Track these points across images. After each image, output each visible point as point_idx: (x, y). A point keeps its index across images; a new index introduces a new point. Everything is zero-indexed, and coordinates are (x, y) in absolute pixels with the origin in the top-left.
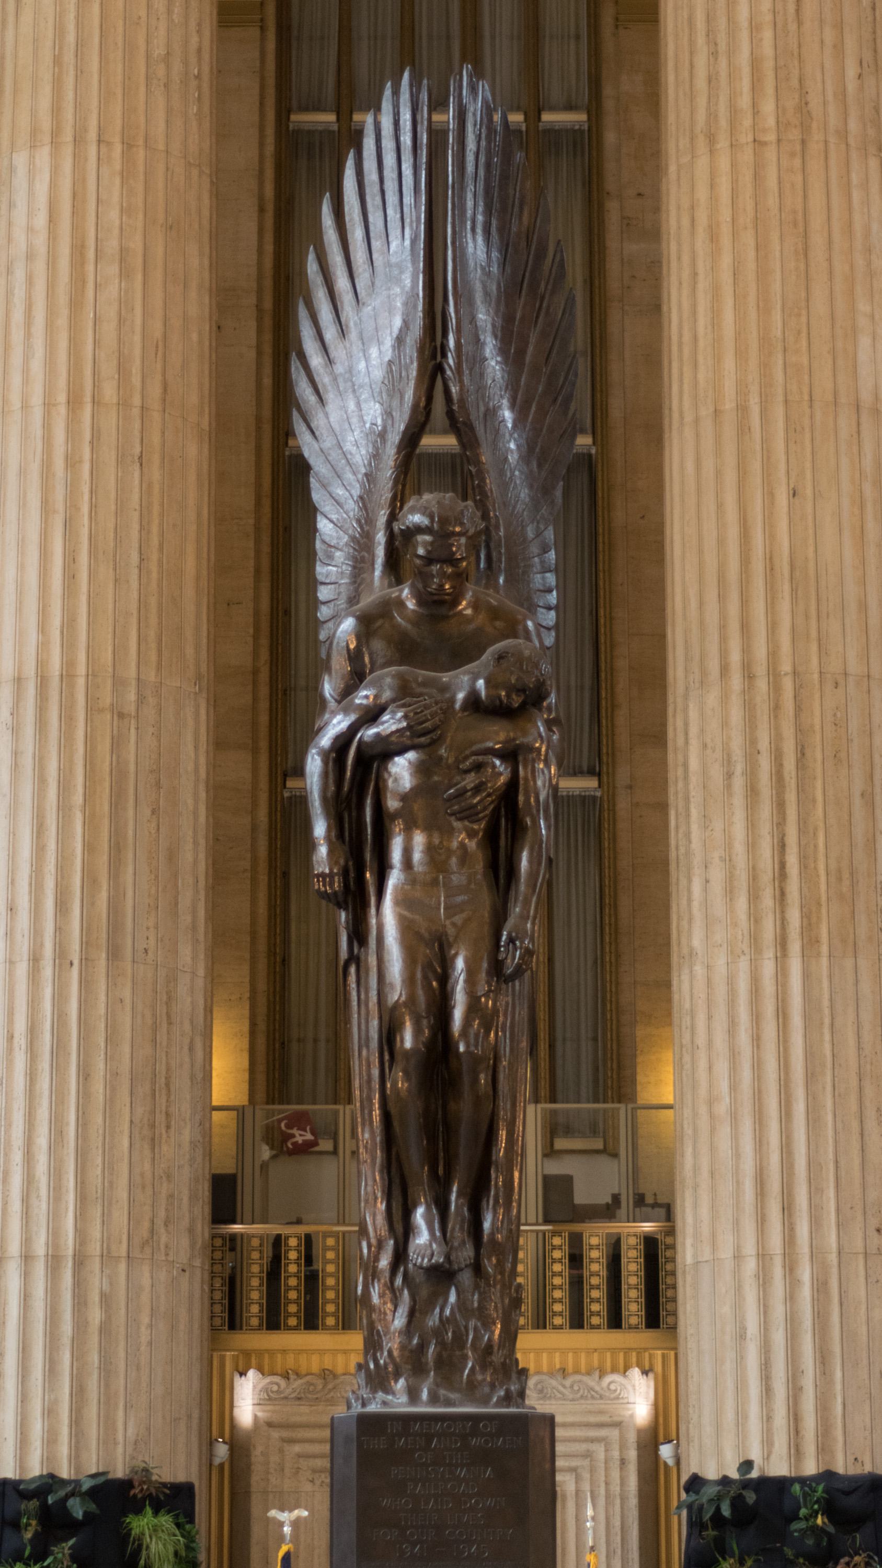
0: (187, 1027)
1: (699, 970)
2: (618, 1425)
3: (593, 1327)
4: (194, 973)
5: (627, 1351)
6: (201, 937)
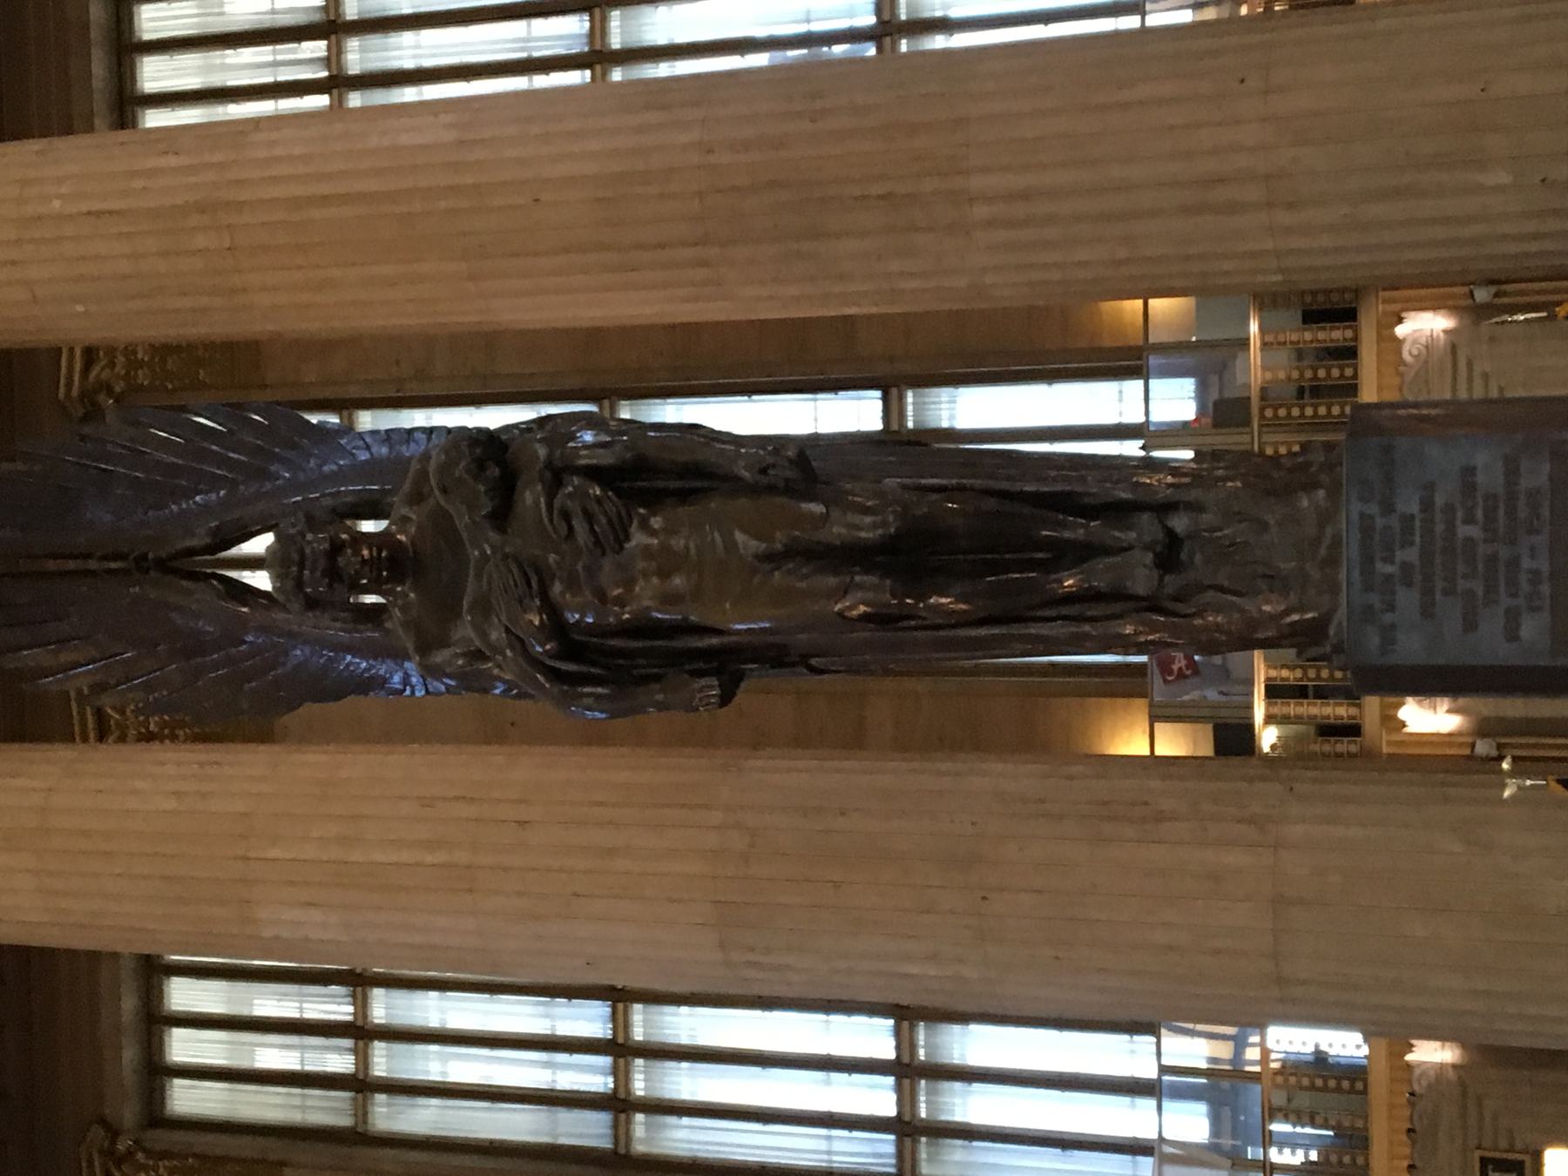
2: (1453, 348)
3: (1355, 376)
5: (1380, 338)
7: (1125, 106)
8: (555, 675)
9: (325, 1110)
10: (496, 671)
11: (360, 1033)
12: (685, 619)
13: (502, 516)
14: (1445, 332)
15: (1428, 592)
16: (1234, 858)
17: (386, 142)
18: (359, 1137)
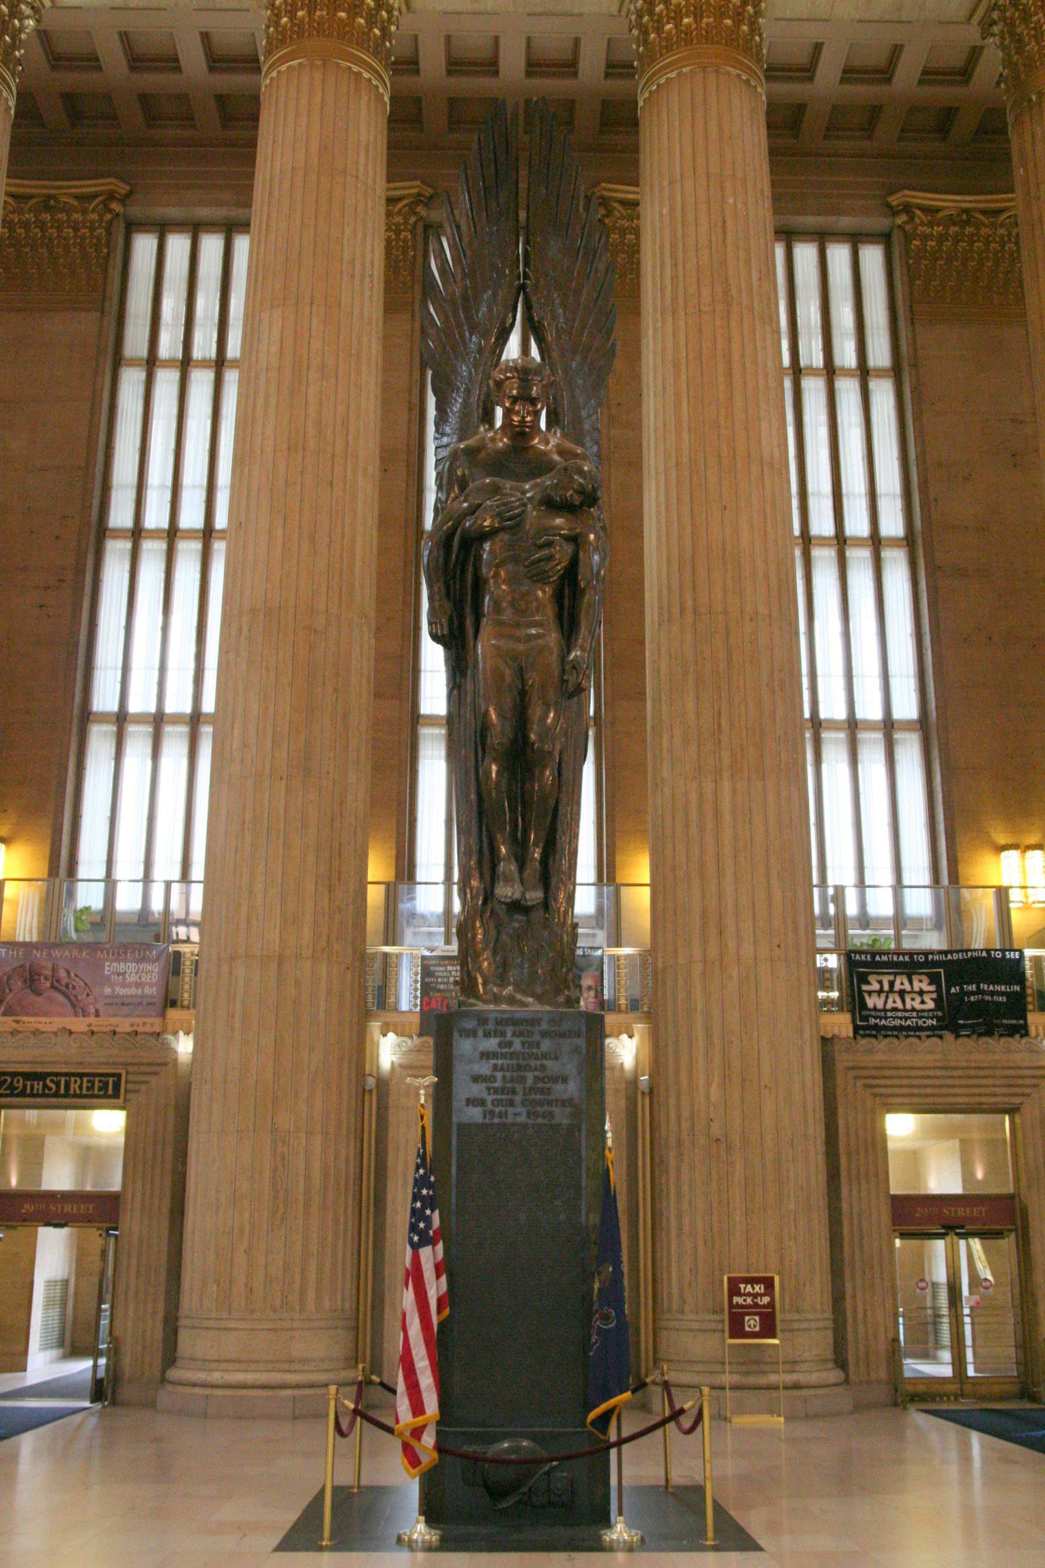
7: (768, 877)
8: (450, 536)
9: (136, 342)
10: (452, 495)
11: (186, 364)
12: (484, 616)
13: (551, 505)
14: (622, 1064)
15: (495, 1055)
16: (307, 933)
18: (118, 361)
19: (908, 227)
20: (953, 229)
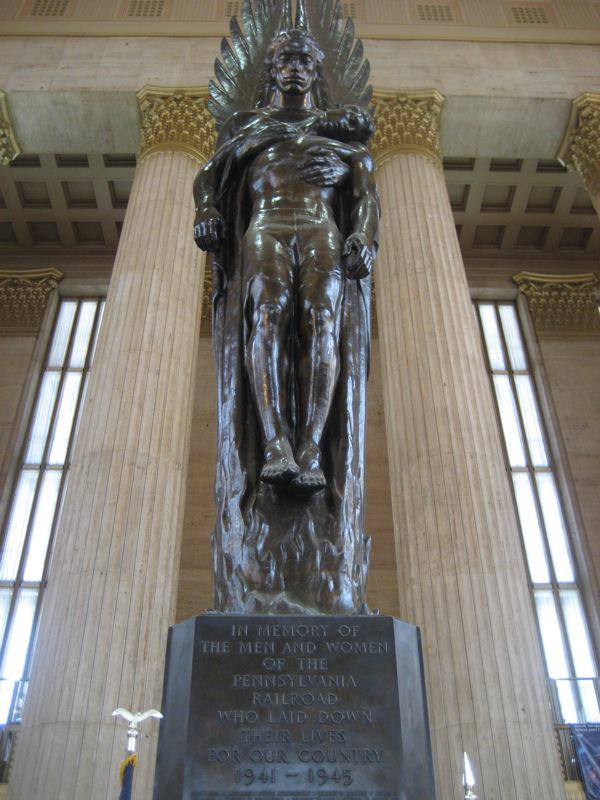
0: (159, 612)
1: (415, 587)
4: (165, 588)
6: (171, 573)
17: (465, 331)
19: (527, 292)
20: (555, 293)
